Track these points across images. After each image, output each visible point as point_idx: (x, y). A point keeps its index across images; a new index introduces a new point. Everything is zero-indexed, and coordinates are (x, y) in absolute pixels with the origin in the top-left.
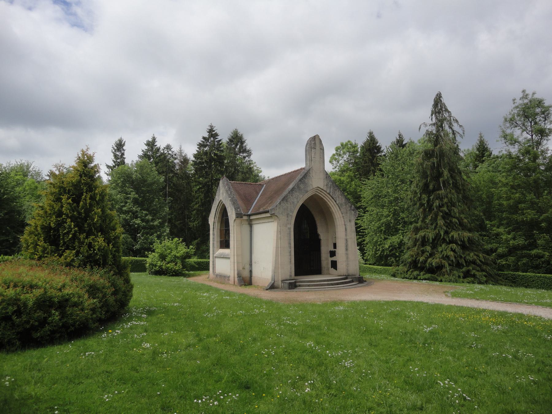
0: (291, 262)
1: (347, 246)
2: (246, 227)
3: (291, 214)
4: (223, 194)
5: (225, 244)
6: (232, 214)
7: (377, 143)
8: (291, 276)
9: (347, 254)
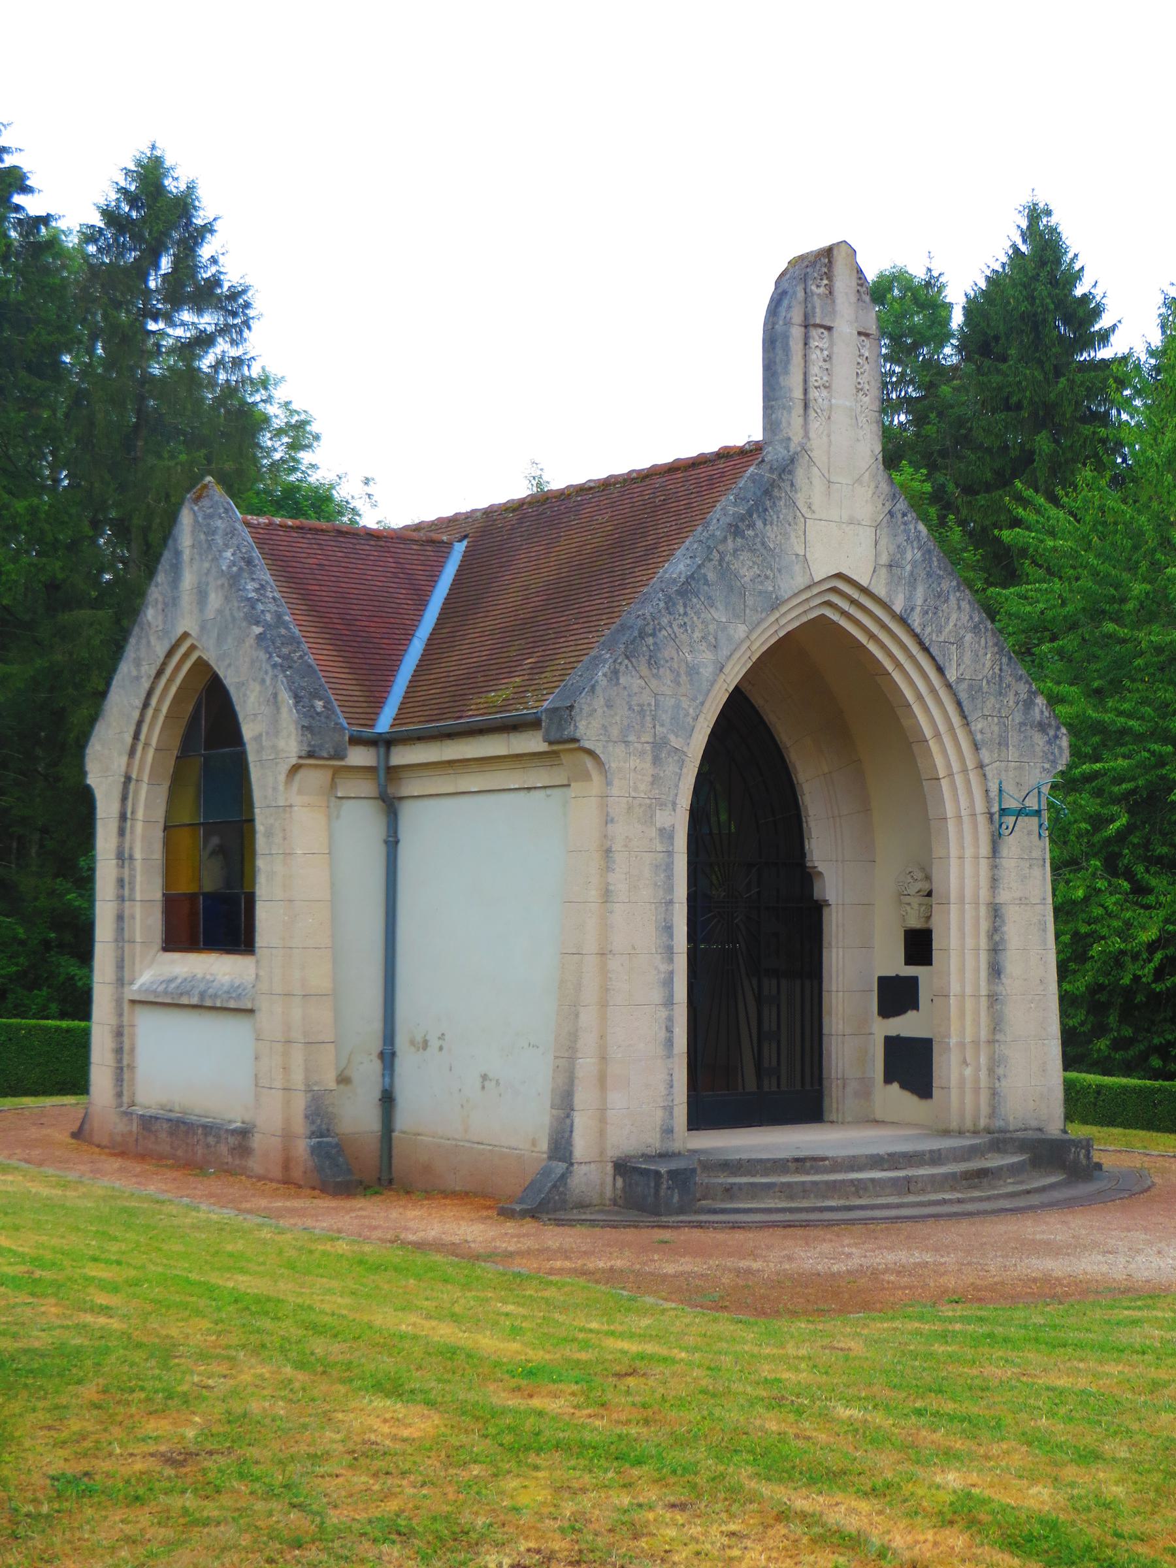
0: (669, 1043)
1: (996, 949)
2: (360, 821)
3: (675, 742)
4: (202, 595)
5: (214, 915)
6: (271, 731)
7: (1077, 276)
8: (668, 1131)
9: (994, 999)
